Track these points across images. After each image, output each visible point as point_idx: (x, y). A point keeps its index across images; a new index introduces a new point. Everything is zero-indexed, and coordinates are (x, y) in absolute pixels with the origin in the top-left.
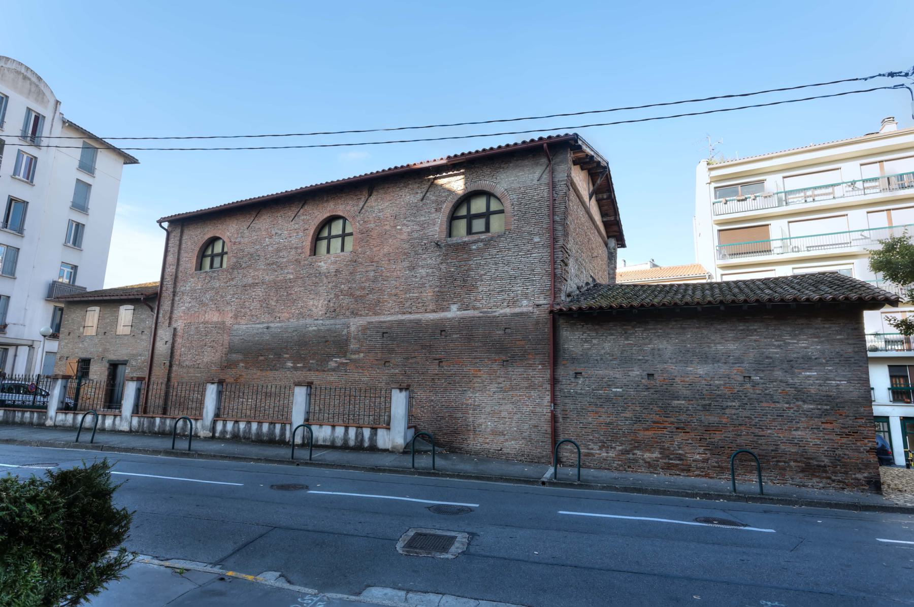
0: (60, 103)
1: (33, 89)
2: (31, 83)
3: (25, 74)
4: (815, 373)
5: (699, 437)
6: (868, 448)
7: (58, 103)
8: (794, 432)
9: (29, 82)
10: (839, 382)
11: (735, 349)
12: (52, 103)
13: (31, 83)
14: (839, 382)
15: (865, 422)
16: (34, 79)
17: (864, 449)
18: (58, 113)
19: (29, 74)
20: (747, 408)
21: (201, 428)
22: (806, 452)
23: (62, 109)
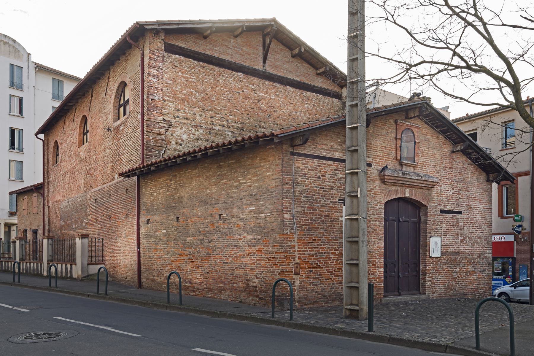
0: (31, 54)
1: (11, 49)
2: (10, 46)
3: (4, 40)
4: (254, 208)
5: (198, 265)
6: (280, 271)
7: (29, 55)
8: (242, 259)
9: (8, 45)
10: (266, 215)
11: (216, 192)
12: (25, 57)
13: (10, 46)
14: (266, 215)
15: (279, 248)
16: (11, 42)
17: (277, 272)
18: (30, 63)
19: (7, 40)
20: (220, 241)
21: (77, 271)
22: (247, 275)
23: (34, 59)
